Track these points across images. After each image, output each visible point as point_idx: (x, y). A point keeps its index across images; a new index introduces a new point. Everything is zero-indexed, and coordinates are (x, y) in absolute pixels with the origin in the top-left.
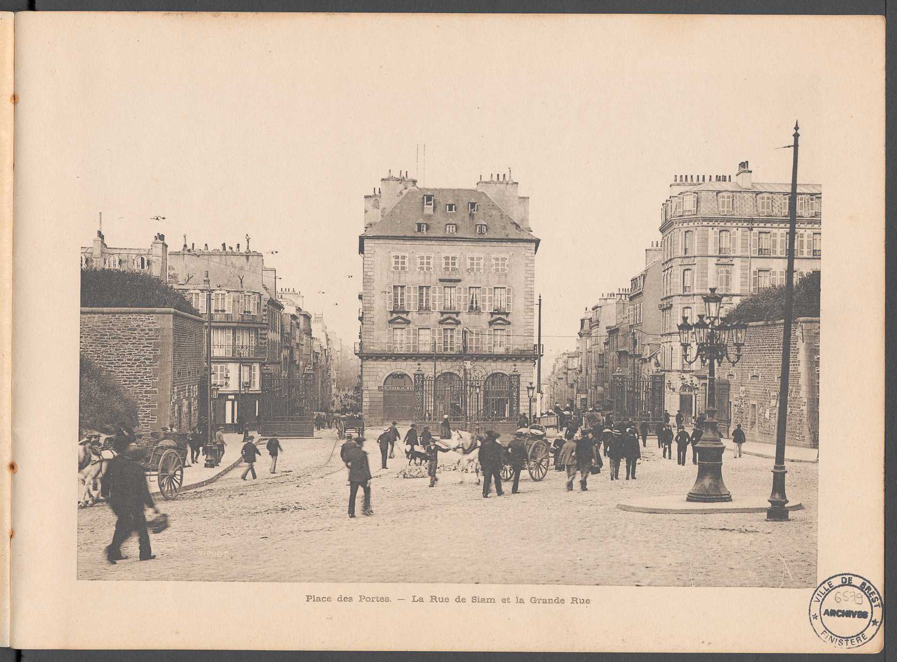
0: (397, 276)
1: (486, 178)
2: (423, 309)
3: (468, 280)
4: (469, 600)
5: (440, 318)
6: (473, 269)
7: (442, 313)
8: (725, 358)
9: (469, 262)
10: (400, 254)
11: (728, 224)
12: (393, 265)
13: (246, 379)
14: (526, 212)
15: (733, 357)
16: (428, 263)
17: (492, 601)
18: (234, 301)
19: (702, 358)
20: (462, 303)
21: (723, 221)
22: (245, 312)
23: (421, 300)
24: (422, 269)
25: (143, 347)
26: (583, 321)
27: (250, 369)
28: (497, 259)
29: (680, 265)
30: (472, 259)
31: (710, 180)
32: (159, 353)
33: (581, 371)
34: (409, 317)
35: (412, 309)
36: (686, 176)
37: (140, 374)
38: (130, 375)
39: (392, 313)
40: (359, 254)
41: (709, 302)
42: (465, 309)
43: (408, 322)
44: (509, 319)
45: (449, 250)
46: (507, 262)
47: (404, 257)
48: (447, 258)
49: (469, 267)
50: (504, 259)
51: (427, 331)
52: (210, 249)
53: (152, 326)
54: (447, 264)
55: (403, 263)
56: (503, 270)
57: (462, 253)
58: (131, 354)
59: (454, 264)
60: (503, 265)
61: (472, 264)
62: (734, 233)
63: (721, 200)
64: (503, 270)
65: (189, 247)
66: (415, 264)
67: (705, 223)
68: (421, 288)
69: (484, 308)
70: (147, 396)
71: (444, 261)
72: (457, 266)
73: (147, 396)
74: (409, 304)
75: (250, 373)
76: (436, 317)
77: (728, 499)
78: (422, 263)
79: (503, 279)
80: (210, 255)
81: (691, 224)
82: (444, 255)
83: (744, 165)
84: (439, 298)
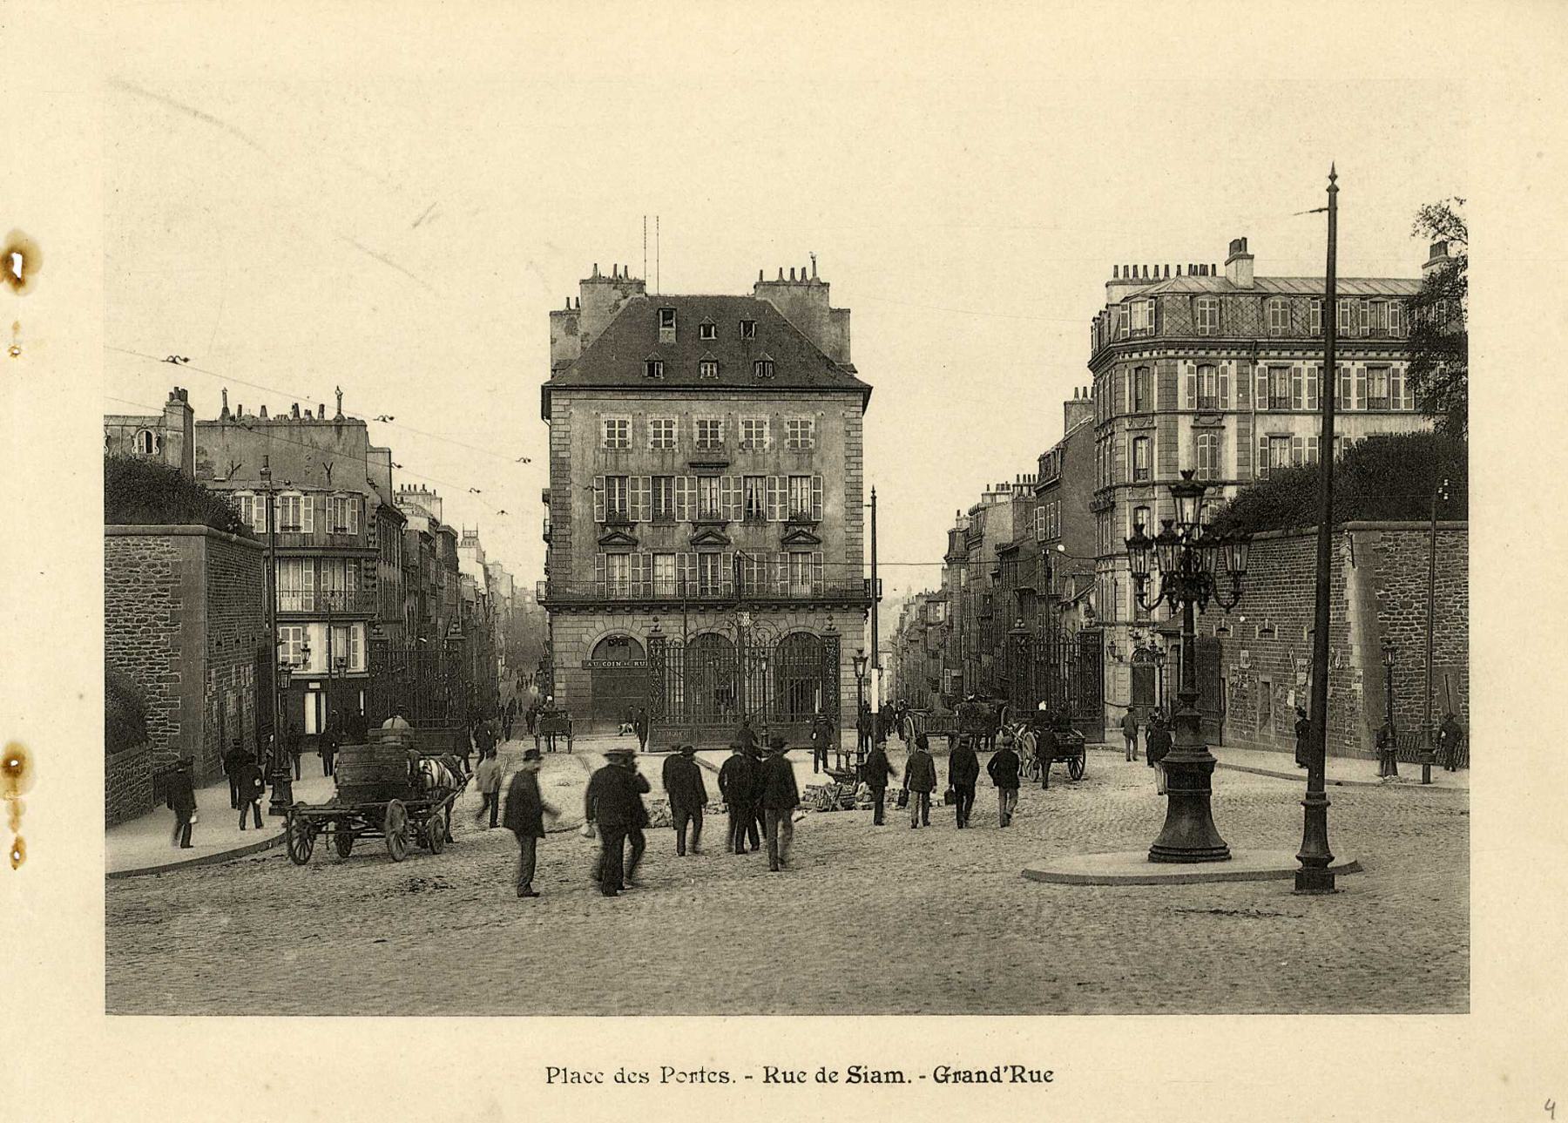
1: (771, 276)
2: (663, 519)
4: (656, 1076)
7: (696, 526)
8: (1212, 600)
10: (617, 418)
11: (1214, 353)
15: (1226, 597)
17: (898, 1077)
18: (316, 510)
19: (1170, 600)
20: (732, 506)
22: (336, 529)
23: (657, 501)
25: (153, 596)
26: (952, 534)
27: (348, 634)
29: (1127, 430)
31: (1179, 273)
33: (951, 627)
34: (637, 533)
36: (1135, 267)
37: (148, 646)
38: (132, 649)
40: (543, 418)
41: (1181, 497)
43: (635, 543)
44: (818, 534)
51: (670, 560)
52: (271, 415)
58: (130, 610)
60: (805, 434)
62: (1224, 370)
65: (233, 411)
67: (1171, 353)
68: (656, 479)
70: (160, 687)
71: (696, 429)
72: (721, 439)
73: (160, 687)
75: (348, 641)
76: (683, 532)
77: (1223, 854)
80: (270, 425)
81: (1146, 355)
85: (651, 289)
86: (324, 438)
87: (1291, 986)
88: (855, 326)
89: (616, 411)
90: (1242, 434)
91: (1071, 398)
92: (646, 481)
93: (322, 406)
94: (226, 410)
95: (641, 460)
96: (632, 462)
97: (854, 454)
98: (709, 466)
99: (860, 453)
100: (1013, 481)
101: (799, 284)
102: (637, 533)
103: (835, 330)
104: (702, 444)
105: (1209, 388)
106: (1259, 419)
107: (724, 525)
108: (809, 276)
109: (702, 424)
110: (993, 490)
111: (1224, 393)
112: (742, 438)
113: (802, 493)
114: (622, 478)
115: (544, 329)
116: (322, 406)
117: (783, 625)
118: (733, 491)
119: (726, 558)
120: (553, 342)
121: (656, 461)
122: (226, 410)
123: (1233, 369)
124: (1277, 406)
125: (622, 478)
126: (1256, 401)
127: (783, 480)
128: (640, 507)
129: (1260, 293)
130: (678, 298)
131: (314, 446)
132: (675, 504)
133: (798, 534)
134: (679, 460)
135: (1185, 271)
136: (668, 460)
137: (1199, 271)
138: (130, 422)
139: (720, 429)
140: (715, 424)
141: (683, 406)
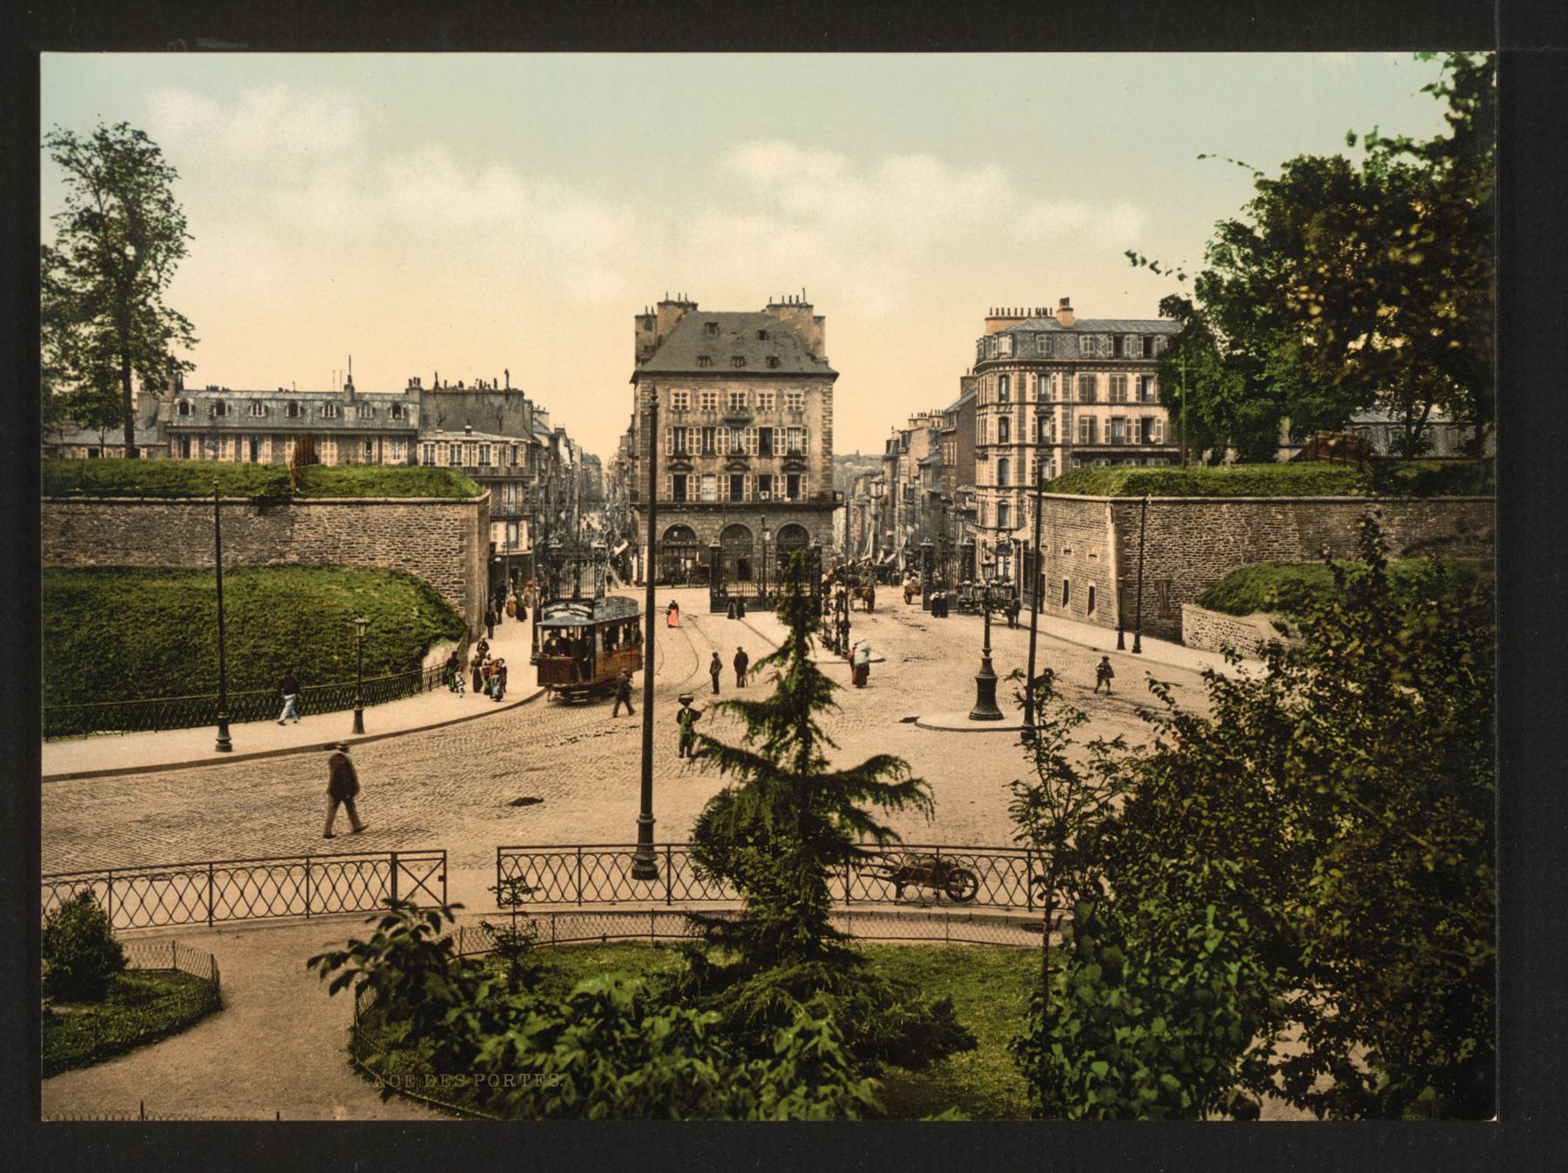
0: (677, 416)
1: (776, 301)
2: (709, 454)
3: (759, 421)
5: (725, 462)
6: (763, 408)
7: (728, 458)
9: (758, 399)
10: (681, 392)
12: (673, 403)
13: (513, 538)
14: (822, 333)
16: (713, 401)
20: (752, 446)
21: (1043, 367)
23: (705, 443)
24: (705, 407)
26: (888, 442)
28: (790, 396)
30: (762, 396)
32: (465, 543)
34: (692, 463)
35: (695, 453)
39: (671, 458)
42: (755, 452)
44: (806, 464)
45: (735, 387)
46: (802, 399)
47: (684, 395)
48: (734, 395)
49: (759, 404)
50: (798, 396)
51: (712, 479)
53: (456, 516)
54: (734, 402)
55: (684, 401)
56: (797, 408)
57: (754, 394)
59: (741, 402)
60: (797, 402)
61: (762, 402)
63: (1038, 341)
64: (797, 408)
65: (441, 385)
66: (697, 402)
69: (777, 451)
71: (730, 398)
72: (745, 405)
74: (691, 449)
76: (721, 462)
77: (1000, 717)
78: (706, 401)
79: (798, 419)
80: (465, 394)
82: (730, 392)
83: (1065, 301)
84: (725, 441)
85: (700, 309)
86: (498, 401)
87: (330, 1056)
88: (828, 325)
89: (681, 387)
90: (1065, 416)
91: (964, 374)
92: (698, 430)
93: (495, 381)
94: (437, 383)
95: (695, 418)
96: (689, 418)
97: (828, 414)
98: (737, 422)
99: (831, 413)
100: (928, 413)
101: (793, 306)
102: (692, 463)
103: (816, 329)
104: (733, 408)
105: (1046, 388)
106: (1076, 408)
107: (747, 458)
108: (801, 301)
109: (734, 395)
110: (915, 417)
111: (1054, 391)
112: (759, 404)
113: (796, 441)
114: (684, 429)
115: (631, 326)
116: (495, 381)
117: (783, 519)
118: (752, 437)
119: (748, 478)
120: (637, 334)
121: (705, 418)
122: (437, 383)
123: (1059, 377)
124: (1089, 399)
125: (684, 429)
126: (1076, 396)
127: (783, 431)
128: (695, 446)
129: (1076, 330)
130: (719, 315)
131: (491, 405)
132: (716, 445)
133: (795, 463)
134: (719, 417)
135: (1033, 314)
136: (712, 417)
137: (1042, 313)
138: (386, 397)
139: (745, 398)
140: (742, 395)
141: (722, 384)
